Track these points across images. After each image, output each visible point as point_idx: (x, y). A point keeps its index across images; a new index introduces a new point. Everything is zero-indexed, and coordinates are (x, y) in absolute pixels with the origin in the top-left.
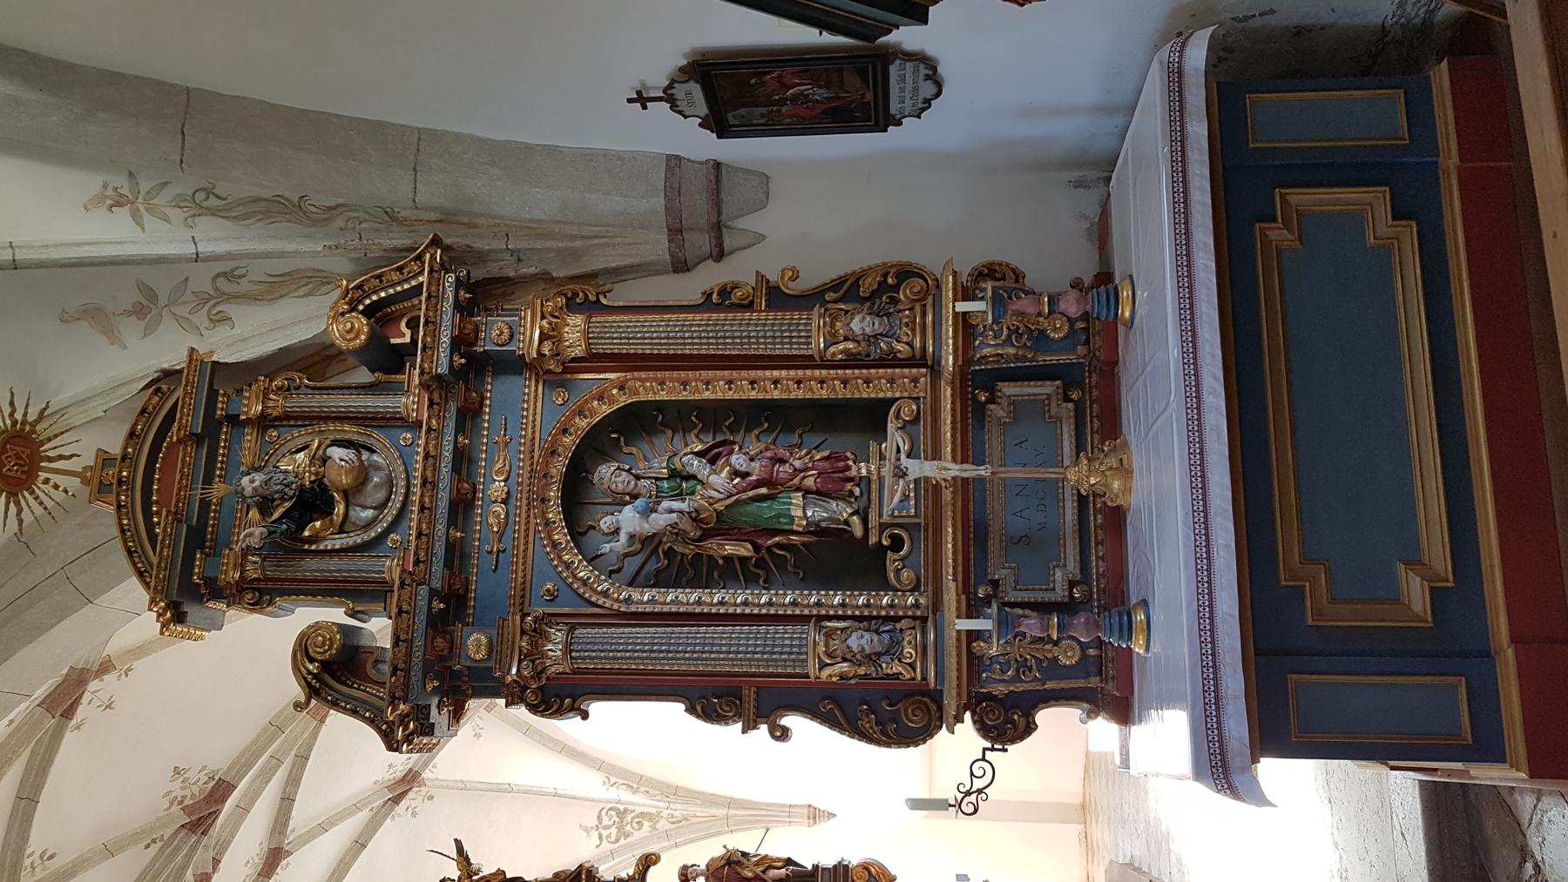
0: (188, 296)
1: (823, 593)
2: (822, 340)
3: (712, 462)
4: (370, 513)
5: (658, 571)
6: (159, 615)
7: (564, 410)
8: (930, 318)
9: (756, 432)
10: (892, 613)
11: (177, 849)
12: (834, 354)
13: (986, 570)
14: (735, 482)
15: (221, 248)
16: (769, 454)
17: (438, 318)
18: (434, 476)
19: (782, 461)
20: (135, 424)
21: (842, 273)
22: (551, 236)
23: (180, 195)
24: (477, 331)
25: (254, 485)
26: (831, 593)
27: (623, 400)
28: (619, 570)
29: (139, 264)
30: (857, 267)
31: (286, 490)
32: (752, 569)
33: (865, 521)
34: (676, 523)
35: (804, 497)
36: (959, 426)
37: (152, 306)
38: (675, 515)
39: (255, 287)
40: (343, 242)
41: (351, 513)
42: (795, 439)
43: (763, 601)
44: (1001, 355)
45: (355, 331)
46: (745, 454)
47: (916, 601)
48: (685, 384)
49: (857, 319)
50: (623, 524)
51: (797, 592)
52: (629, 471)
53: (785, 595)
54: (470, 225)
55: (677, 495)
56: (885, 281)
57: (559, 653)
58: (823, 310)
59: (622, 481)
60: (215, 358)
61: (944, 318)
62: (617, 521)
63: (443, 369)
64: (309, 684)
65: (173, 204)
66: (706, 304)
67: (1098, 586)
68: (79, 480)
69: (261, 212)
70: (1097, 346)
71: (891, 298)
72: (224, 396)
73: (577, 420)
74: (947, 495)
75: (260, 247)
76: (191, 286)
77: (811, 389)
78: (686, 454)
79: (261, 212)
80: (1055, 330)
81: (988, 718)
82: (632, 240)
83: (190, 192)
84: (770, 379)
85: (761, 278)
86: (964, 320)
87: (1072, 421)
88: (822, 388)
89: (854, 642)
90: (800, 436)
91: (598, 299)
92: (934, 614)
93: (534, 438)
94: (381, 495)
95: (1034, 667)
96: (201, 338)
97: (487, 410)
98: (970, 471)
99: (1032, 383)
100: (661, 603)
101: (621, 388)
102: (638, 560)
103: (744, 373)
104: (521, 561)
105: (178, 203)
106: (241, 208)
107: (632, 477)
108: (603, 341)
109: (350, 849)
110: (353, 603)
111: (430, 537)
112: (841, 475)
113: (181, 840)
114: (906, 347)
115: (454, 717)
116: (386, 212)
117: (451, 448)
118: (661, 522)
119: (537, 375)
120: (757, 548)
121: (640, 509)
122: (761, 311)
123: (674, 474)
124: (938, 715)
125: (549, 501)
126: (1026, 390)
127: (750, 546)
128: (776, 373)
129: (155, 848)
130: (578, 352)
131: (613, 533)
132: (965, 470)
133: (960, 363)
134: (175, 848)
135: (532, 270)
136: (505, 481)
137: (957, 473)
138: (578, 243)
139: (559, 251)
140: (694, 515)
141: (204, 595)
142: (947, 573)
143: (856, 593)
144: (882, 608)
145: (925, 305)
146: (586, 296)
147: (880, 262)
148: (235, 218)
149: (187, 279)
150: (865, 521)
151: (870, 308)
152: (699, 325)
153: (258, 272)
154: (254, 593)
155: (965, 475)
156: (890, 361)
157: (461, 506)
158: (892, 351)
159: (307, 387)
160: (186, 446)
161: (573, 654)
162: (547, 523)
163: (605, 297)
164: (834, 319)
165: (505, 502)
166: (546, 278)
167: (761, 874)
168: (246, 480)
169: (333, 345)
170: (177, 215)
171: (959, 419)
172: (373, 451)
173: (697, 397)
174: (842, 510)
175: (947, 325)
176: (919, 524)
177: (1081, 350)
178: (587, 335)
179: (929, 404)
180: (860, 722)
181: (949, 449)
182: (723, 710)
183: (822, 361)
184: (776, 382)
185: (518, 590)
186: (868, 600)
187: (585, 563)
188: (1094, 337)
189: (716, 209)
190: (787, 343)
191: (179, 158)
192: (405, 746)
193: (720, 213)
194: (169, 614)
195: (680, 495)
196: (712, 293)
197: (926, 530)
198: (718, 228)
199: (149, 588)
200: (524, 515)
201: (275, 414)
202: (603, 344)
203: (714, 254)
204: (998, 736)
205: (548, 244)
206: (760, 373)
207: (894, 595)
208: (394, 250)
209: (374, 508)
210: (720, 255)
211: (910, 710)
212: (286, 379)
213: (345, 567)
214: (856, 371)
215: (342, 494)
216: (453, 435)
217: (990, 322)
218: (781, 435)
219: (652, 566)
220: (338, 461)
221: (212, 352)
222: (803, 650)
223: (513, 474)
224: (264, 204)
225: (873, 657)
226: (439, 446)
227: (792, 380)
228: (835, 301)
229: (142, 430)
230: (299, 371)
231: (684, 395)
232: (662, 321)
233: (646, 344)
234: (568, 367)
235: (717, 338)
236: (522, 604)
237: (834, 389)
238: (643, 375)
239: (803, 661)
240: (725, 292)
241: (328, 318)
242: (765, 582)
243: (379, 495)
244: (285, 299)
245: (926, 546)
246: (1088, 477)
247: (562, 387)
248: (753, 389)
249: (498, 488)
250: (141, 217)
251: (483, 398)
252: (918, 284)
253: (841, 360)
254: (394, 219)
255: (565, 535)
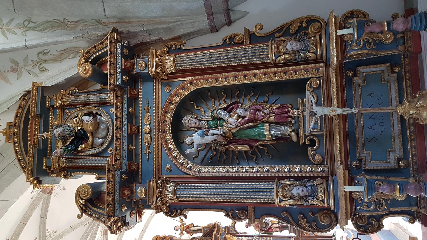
0: (30, 62)
1: (280, 166)
2: (274, 55)
3: (230, 112)
4: (101, 140)
5: (212, 157)
6: (31, 183)
7: (169, 94)
8: (324, 40)
9: (249, 97)
10: (312, 175)
11: (93, 226)
12: (279, 61)
13: (356, 155)
14: (239, 120)
15: (35, 42)
16: (253, 108)
17: (116, 62)
18: (121, 125)
19: (259, 110)
20: (18, 112)
21: (282, 24)
22: (161, 23)
23: (19, 23)
24: (133, 65)
25: (58, 132)
26: (284, 166)
27: (193, 89)
28: (197, 157)
29: (7, 52)
30: (288, 21)
31: (71, 133)
32: (250, 155)
33: (297, 135)
34: (216, 139)
35: (269, 125)
36: (340, 88)
37: (17, 68)
38: (214, 136)
39: (54, 56)
40: (81, 35)
41: (95, 141)
42: (265, 99)
43: (254, 170)
44: (360, 54)
45: (87, 70)
46: (242, 108)
47: (323, 169)
48: (217, 79)
49: (289, 44)
50: (194, 141)
51: (269, 166)
52: (196, 118)
53: (264, 167)
54: (129, 22)
55: (216, 127)
56: (302, 25)
57: (171, 195)
58: (273, 41)
59: (193, 123)
60: (43, 85)
61: (331, 39)
62: (192, 140)
63: (119, 82)
64: (82, 208)
65: (17, 27)
66: (224, 44)
67: (412, 160)
68: (2, 134)
69: (50, 27)
70: (409, 45)
71: (305, 33)
72: (49, 98)
73: (175, 98)
74: (336, 122)
75: (49, 40)
76: (30, 59)
77: (271, 77)
78: (218, 110)
79: (50, 27)
80: (387, 39)
81: (359, 222)
82: (192, 21)
83: (22, 22)
84: (252, 74)
85: (246, 30)
86: (341, 40)
87: (396, 82)
88: (275, 76)
89: (295, 191)
90: (268, 97)
91: (181, 47)
92: (332, 175)
93: (159, 107)
94: (104, 133)
95: (384, 204)
96: (38, 77)
97: (141, 97)
98: (347, 111)
99: (375, 66)
100: (212, 172)
101: (191, 83)
102: (204, 153)
103: (240, 73)
104: (157, 157)
105: (19, 26)
106: (42, 26)
107: (197, 120)
108: (181, 65)
109: (150, 217)
110: (98, 174)
111: (121, 149)
112: (285, 115)
113: (94, 224)
114: (313, 54)
115: (139, 216)
116: (97, 21)
117: (126, 113)
118: (210, 139)
119: (158, 81)
120: (251, 147)
121: (200, 135)
122: (247, 45)
123: (214, 118)
124: (335, 219)
125: (167, 131)
126: (375, 69)
127: (248, 147)
128: (255, 72)
129: (87, 226)
130: (172, 70)
131: (191, 144)
132: (345, 111)
133: (340, 60)
134: (92, 226)
135: (155, 38)
136: (149, 125)
137: (341, 113)
138: (171, 25)
139: (165, 29)
140: (223, 135)
141: (49, 172)
142: (337, 157)
143: (295, 166)
144: (307, 172)
145: (321, 34)
146: (176, 46)
147: (299, 17)
148: (40, 30)
149: (28, 56)
150: (297, 135)
151: (295, 38)
152: (220, 54)
153: (53, 50)
154: (65, 172)
155: (345, 113)
156: (306, 61)
157: (134, 136)
158: (306, 57)
159: (78, 92)
160: (36, 119)
161: (177, 196)
162: (166, 141)
163: (184, 46)
164: (279, 45)
165: (149, 133)
166: (160, 41)
167: (271, 226)
168: (55, 131)
169: (80, 76)
170: (19, 31)
171: (340, 86)
172: (101, 116)
173: (222, 85)
174: (287, 130)
175: (333, 42)
176: (323, 134)
177: (401, 48)
178: (174, 62)
179: (325, 80)
180: (299, 222)
181: (336, 100)
182: (240, 216)
183: (275, 64)
184: (255, 75)
185: (157, 168)
186: (301, 169)
187: (182, 156)
188: (407, 40)
189: (226, 3)
190: (258, 58)
191: (13, 8)
192: (118, 231)
193: (228, 5)
194: (35, 182)
195: (217, 127)
196: (226, 39)
197: (326, 137)
198: (228, 11)
199: (26, 173)
200: (157, 138)
201: (66, 104)
202: (182, 66)
203: (227, 22)
204: (364, 230)
205: (159, 26)
206: (247, 72)
207: (313, 166)
208: (101, 36)
209: (102, 138)
210: (230, 23)
211: (322, 217)
212: (70, 90)
213: (93, 162)
214: (290, 67)
215: (90, 133)
216: (127, 108)
217: (356, 38)
218: (259, 97)
219: (210, 155)
220: (86, 122)
221: (42, 83)
222: (272, 194)
223: (152, 122)
224: (51, 23)
225: (304, 198)
226: (122, 113)
227: (262, 74)
228: (279, 37)
229: (20, 114)
230: (76, 87)
231: (217, 84)
232: (204, 54)
233: (199, 64)
234: (169, 76)
235: (228, 59)
236: (159, 173)
237: (281, 76)
238: (199, 77)
239: (272, 198)
240: (232, 38)
241: (78, 66)
242: (256, 160)
243: (103, 133)
244: (66, 60)
245: (326, 144)
246: (409, 111)
247: (169, 85)
248: (245, 79)
249: (146, 128)
250: (5, 34)
251: (139, 92)
252: (317, 25)
253: (283, 63)
254: (100, 23)
255: (173, 145)
